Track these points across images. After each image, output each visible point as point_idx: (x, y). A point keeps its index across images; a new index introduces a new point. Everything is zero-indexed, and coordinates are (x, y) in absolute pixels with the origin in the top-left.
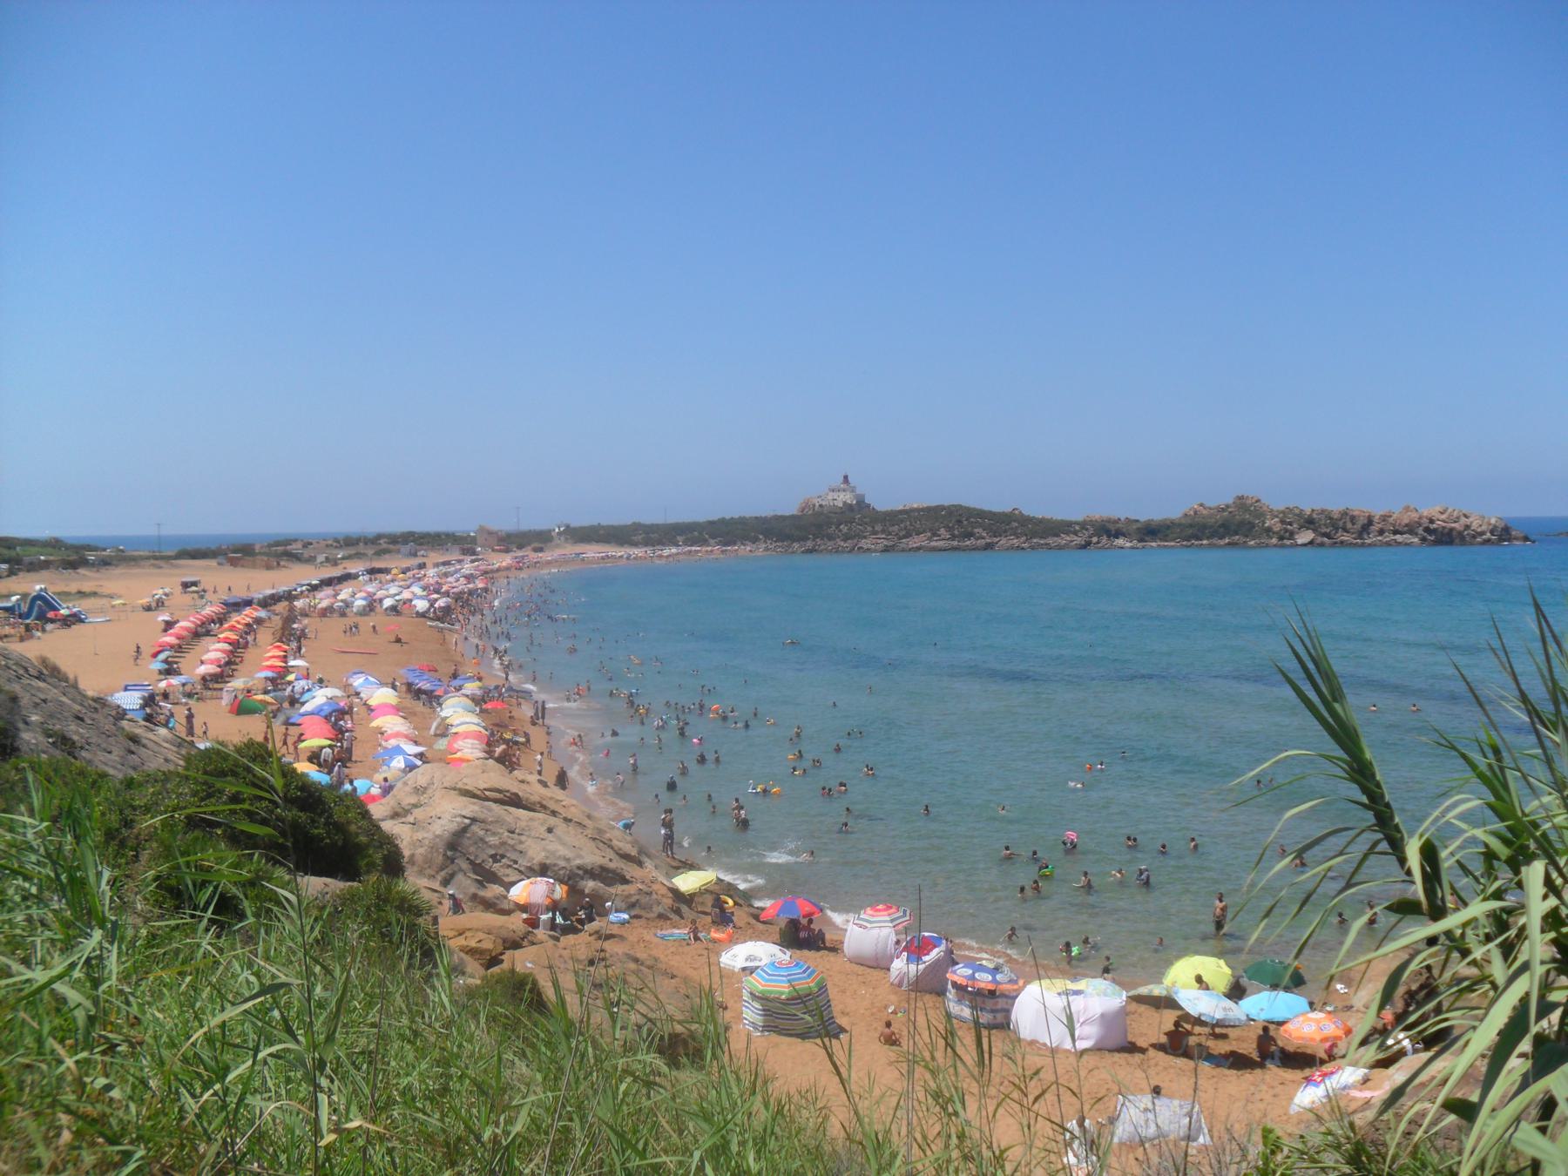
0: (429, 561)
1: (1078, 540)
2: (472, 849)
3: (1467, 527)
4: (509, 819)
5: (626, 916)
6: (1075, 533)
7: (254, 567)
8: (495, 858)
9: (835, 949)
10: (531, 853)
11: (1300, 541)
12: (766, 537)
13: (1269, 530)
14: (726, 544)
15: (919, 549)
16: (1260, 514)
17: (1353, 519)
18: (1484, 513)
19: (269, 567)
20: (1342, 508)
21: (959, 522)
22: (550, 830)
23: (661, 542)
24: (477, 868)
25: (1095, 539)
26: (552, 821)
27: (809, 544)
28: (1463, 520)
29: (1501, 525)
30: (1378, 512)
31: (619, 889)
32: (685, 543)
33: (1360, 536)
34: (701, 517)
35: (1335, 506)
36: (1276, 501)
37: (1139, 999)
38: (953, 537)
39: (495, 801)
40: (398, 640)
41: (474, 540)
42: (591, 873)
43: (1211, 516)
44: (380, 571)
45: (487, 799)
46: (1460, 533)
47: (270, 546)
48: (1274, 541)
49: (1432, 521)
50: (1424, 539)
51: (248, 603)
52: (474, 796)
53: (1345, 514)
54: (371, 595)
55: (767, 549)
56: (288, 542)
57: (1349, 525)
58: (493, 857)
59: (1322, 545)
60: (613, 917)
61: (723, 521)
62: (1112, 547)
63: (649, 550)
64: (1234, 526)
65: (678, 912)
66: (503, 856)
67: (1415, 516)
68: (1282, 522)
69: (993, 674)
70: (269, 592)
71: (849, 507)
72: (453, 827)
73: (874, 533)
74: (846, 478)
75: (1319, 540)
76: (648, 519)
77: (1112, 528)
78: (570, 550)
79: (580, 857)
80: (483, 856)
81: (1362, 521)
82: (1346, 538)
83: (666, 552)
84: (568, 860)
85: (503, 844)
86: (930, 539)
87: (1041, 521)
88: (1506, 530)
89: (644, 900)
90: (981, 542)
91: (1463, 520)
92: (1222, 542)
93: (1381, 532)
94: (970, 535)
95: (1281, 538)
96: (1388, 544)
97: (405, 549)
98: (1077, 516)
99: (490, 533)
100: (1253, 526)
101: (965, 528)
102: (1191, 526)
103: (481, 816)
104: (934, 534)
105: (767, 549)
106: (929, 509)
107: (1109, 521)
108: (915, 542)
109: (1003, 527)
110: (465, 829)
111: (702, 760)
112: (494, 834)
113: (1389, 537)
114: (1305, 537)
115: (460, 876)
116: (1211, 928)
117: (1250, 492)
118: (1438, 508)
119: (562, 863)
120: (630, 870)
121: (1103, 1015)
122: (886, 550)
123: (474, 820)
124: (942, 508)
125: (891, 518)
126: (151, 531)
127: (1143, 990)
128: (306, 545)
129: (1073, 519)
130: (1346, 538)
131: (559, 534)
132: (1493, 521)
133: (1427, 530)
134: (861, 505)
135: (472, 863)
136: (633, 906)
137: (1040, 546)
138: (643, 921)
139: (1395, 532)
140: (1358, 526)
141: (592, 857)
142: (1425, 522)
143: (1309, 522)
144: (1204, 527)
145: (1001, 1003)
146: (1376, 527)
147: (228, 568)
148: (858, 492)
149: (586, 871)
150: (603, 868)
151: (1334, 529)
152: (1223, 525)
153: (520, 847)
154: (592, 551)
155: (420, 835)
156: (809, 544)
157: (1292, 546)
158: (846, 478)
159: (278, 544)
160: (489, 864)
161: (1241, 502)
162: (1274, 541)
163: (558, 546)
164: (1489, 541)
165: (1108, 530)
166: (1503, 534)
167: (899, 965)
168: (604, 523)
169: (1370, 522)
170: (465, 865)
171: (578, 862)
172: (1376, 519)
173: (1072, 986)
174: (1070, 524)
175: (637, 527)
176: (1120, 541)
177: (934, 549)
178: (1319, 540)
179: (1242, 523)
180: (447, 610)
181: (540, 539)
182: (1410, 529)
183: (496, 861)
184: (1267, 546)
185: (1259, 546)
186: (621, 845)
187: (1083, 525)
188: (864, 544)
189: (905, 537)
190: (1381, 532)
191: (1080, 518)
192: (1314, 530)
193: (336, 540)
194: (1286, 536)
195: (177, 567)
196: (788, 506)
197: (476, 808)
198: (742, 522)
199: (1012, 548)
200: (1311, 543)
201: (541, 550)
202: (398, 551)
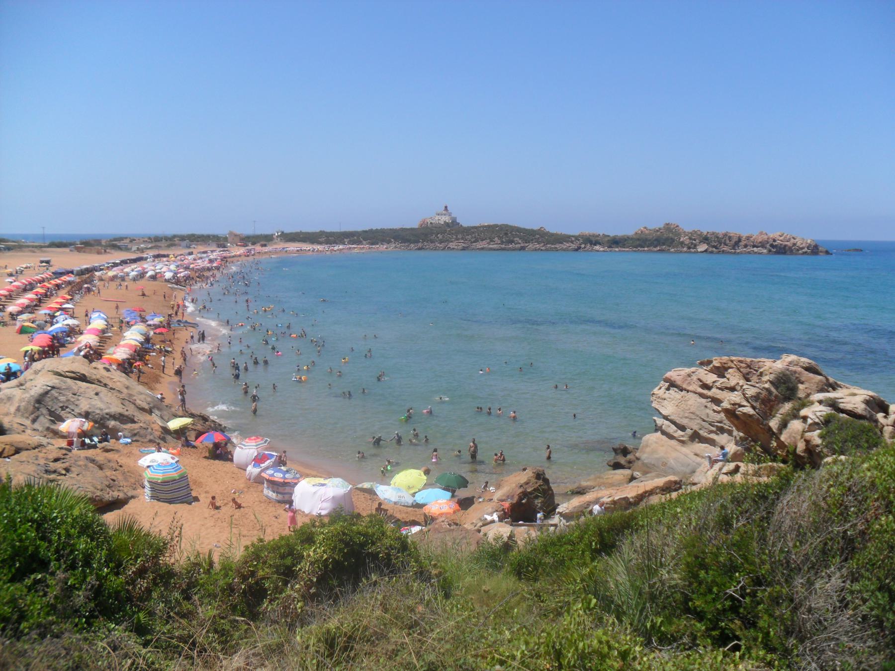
0: (195, 251)
1: (574, 246)
2: (50, 403)
3: (794, 244)
4: (75, 388)
5: (129, 440)
6: (572, 242)
7: (90, 253)
8: (63, 408)
9: (231, 460)
10: (82, 406)
11: (699, 250)
12: (396, 240)
13: (682, 243)
14: (372, 244)
15: (482, 249)
16: (678, 234)
17: (730, 238)
18: (804, 237)
19: (99, 253)
20: (724, 232)
21: (506, 234)
22: (97, 394)
23: (335, 243)
24: (52, 413)
25: (583, 246)
26: (99, 388)
27: (420, 245)
28: (792, 240)
29: (813, 244)
30: (744, 234)
31: (129, 426)
32: (349, 243)
33: (734, 248)
34: (360, 229)
35: (720, 230)
36: (687, 227)
37: (357, 488)
38: (502, 243)
39: (71, 378)
40: (144, 295)
41: (226, 239)
42: (113, 417)
43: (650, 234)
44: (164, 256)
45: (67, 377)
46: (790, 248)
47: (111, 241)
48: (685, 249)
49: (774, 241)
50: (770, 251)
51: (72, 272)
52: (61, 375)
53: (725, 235)
54: (144, 269)
55: (396, 247)
56: (121, 239)
57: (728, 242)
58: (61, 407)
59: (712, 252)
60: (122, 441)
61: (371, 231)
62: (592, 250)
63: (326, 247)
64: (663, 240)
65: (164, 439)
66: (67, 407)
67: (765, 237)
68: (690, 239)
69: (612, 325)
70: (85, 267)
71: (447, 224)
72: (41, 391)
73: (457, 239)
74: (446, 207)
75: (711, 249)
76: (328, 229)
77: (593, 239)
78: (280, 245)
79: (109, 408)
80: (56, 407)
81: (735, 240)
82: (726, 248)
83: (336, 248)
84: (101, 410)
85: (68, 400)
86: (489, 243)
87: (553, 235)
88: (816, 246)
89: (142, 432)
90: (518, 246)
91: (792, 240)
92: (655, 249)
93: (746, 246)
94: (512, 242)
95: (689, 248)
96: (749, 253)
97: (184, 243)
98: (576, 233)
99: (236, 235)
100: (673, 240)
101: (508, 237)
102: (638, 239)
103: (58, 385)
104: (492, 241)
105: (396, 247)
106: (489, 226)
107: (594, 236)
108: (480, 245)
109: (531, 237)
110: (47, 393)
111: (256, 363)
112: (64, 395)
113: (750, 249)
114: (702, 247)
115: (41, 418)
116: (469, 458)
117: (673, 221)
118: (779, 233)
119: (98, 411)
120: (139, 416)
121: (333, 497)
122: (464, 249)
123: (53, 388)
124: (496, 226)
125: (468, 231)
126: (39, 232)
127: (360, 486)
128: (132, 241)
129: (571, 234)
130: (726, 248)
131: (278, 236)
132: (809, 241)
133: (772, 245)
134: (454, 222)
135: (49, 410)
136: (135, 435)
137: (551, 250)
138: (139, 443)
139: (754, 246)
140: (733, 242)
141: (116, 408)
142: (771, 241)
143: (705, 239)
144: (647, 240)
145: (287, 489)
146: (742, 243)
147: (76, 253)
148: (453, 215)
149: (111, 416)
150: (121, 415)
151: (718, 243)
152: (656, 240)
153: (77, 403)
154: (293, 247)
155: (24, 396)
156: (420, 245)
157: (695, 252)
158: (446, 207)
159: (115, 240)
160: (59, 411)
161: (668, 227)
162: (685, 249)
163: (276, 243)
164: (805, 253)
165: (591, 241)
166: (814, 250)
167: (250, 468)
168: (304, 231)
169: (740, 240)
170: (44, 411)
171: (107, 411)
172: (743, 239)
173: (322, 481)
174: (570, 237)
175: (322, 233)
176: (597, 247)
177: (491, 249)
178: (711, 249)
179: (667, 239)
180: (187, 278)
181: (266, 239)
182: (762, 245)
183: (63, 410)
184: (681, 252)
185: (676, 252)
186: (140, 402)
187: (577, 238)
188: (452, 245)
189: (474, 242)
190: (746, 246)
191: (577, 233)
192: (708, 244)
193: (150, 238)
194: (692, 246)
195: (45, 252)
196: (413, 223)
197: (57, 381)
198: (383, 231)
199: (536, 250)
200: (706, 251)
201: (265, 245)
202: (180, 245)
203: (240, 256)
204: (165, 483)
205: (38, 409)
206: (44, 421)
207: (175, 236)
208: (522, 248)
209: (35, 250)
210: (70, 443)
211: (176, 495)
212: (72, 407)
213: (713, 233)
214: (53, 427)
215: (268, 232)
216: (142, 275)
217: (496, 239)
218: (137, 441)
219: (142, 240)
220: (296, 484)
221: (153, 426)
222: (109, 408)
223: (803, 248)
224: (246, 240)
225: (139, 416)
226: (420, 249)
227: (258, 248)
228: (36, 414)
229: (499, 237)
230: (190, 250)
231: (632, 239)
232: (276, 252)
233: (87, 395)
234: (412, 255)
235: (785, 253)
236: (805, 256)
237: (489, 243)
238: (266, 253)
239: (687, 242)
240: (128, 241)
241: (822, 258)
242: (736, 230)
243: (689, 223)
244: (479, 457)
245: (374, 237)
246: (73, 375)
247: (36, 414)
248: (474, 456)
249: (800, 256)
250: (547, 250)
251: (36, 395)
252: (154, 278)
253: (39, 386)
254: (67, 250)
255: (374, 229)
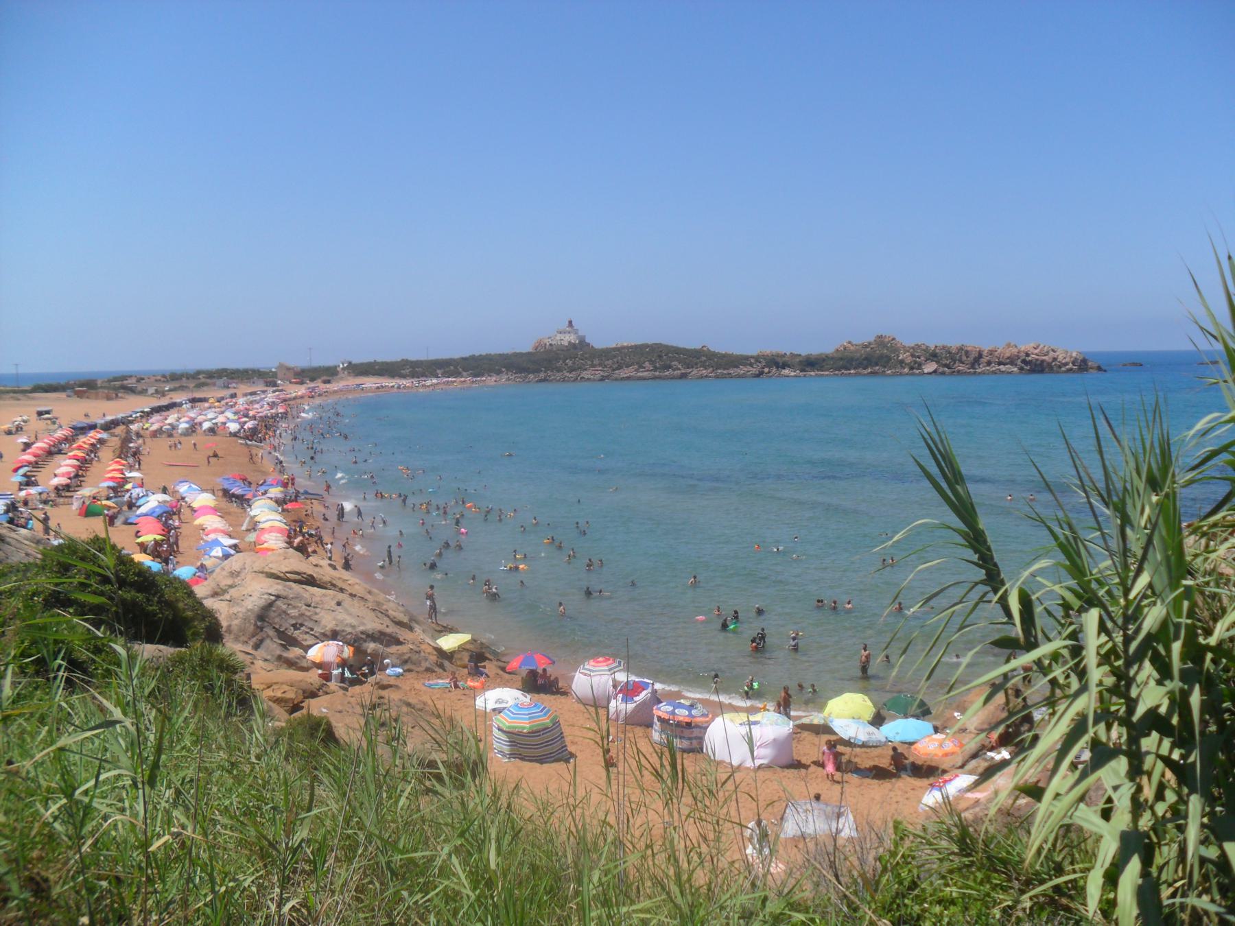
1: (754, 371)
2: (277, 620)
3: (1055, 359)
4: (306, 595)
5: (400, 670)
6: (751, 365)
7: (97, 398)
10: (324, 622)
11: (926, 371)
13: (902, 362)
14: (476, 376)
15: (628, 378)
16: (896, 350)
17: (967, 353)
18: (1067, 348)
19: (109, 398)
20: (959, 344)
21: (660, 357)
22: (339, 604)
24: (281, 634)
25: (766, 370)
27: (542, 375)
28: (1051, 354)
30: (986, 348)
31: (393, 649)
33: (973, 366)
35: (953, 343)
38: (655, 369)
39: (295, 581)
41: (275, 375)
42: (372, 637)
43: (857, 351)
45: (288, 580)
46: (1049, 364)
48: (906, 370)
49: (1028, 355)
50: (1021, 369)
52: (278, 578)
55: (508, 379)
56: (124, 378)
57: (964, 358)
58: (294, 625)
59: (943, 373)
61: (473, 358)
63: (415, 381)
66: (302, 625)
67: (1015, 351)
68: (912, 355)
71: (573, 346)
72: (262, 603)
73: (593, 366)
74: (570, 322)
75: (941, 369)
76: (413, 357)
77: (780, 361)
78: (353, 381)
79: (364, 624)
80: (286, 625)
81: (974, 355)
83: (429, 382)
84: (353, 627)
85: (302, 615)
86: (637, 370)
87: (724, 356)
88: (1084, 361)
89: (415, 657)
90: (677, 373)
91: (1051, 354)
92: (865, 372)
93: (989, 363)
94: (668, 367)
95: (912, 368)
96: (994, 373)
99: (288, 369)
100: (889, 359)
101: (664, 361)
104: (641, 367)
105: (508, 379)
106: (636, 347)
107: (778, 355)
108: (624, 373)
109: (695, 360)
110: (271, 605)
112: (294, 607)
113: (995, 367)
114: (930, 367)
115: (268, 642)
117: (887, 333)
118: (1032, 345)
119: (349, 630)
120: (403, 634)
122: (602, 379)
123: (278, 597)
124: (646, 346)
125: (606, 354)
128: (140, 380)
129: (750, 354)
131: (343, 369)
132: (1074, 355)
133: (1024, 361)
135: (277, 630)
136: (406, 662)
137: (723, 376)
139: (1000, 364)
141: (372, 624)
142: (1023, 356)
143: (933, 356)
145: (696, 732)
146: (984, 360)
149: (368, 636)
150: (382, 633)
152: (866, 359)
153: (315, 618)
154: (370, 382)
156: (542, 375)
158: (570, 322)
159: (115, 379)
160: (291, 631)
162: (906, 370)
163: (342, 379)
164: (1070, 370)
165: (777, 363)
166: (1082, 365)
168: (379, 360)
169: (980, 355)
170: (271, 633)
171: (362, 628)
172: (985, 353)
174: (747, 358)
175: (405, 363)
176: (786, 371)
178: (941, 369)
179: (881, 357)
181: (329, 373)
182: (1011, 361)
183: (296, 629)
184: (901, 374)
185: (894, 374)
187: (757, 359)
188: (585, 374)
189: (617, 369)
190: (989, 363)
191: (755, 353)
192: (937, 362)
193: (164, 376)
194: (915, 366)
195: (33, 399)
196: (525, 345)
197: (280, 587)
199: (702, 377)
200: (935, 372)
201: (329, 382)
202: (214, 384)
203: (302, 397)
204: (533, 733)
205: (261, 629)
206: (272, 646)
207: (199, 372)
208: (683, 376)
209: (18, 395)
210: (327, 677)
211: (548, 750)
212: (310, 624)
213: (944, 347)
214: (285, 655)
215: (329, 362)
216: (193, 428)
217: (647, 364)
218: (409, 671)
219: (153, 379)
220: (709, 723)
221: (423, 647)
222: (364, 624)
223: (1066, 364)
224: (303, 375)
225: (403, 634)
226: (541, 381)
227: (320, 386)
228: (259, 637)
229: (651, 362)
230: (232, 391)
231: (832, 358)
232: (348, 390)
233: (327, 607)
234: (534, 390)
235: (1042, 371)
236: (1071, 375)
237: (637, 370)
238: (335, 392)
239: (909, 360)
240: (134, 380)
241: (1091, 377)
242: (976, 342)
243: (604, 335)
244: (870, 672)
245: (477, 366)
246: (297, 577)
247: (259, 637)
248: (864, 669)
249: (1064, 376)
250: (717, 377)
251: (256, 609)
252: (212, 430)
253: (256, 595)
254: (63, 395)
255: (477, 354)
